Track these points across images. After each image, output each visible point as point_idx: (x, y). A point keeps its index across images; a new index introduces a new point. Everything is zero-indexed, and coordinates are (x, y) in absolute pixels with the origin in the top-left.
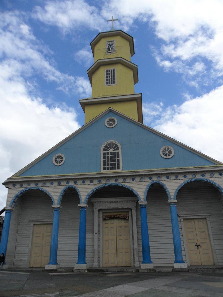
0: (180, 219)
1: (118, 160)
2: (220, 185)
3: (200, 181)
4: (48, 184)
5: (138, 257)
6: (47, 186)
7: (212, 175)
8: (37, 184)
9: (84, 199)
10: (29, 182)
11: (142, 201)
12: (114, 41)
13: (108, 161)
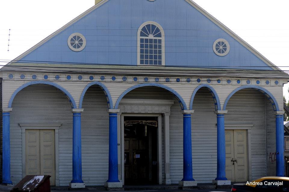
2: (274, 96)
6: (73, 79)
11: (188, 108)
13: (155, 52)
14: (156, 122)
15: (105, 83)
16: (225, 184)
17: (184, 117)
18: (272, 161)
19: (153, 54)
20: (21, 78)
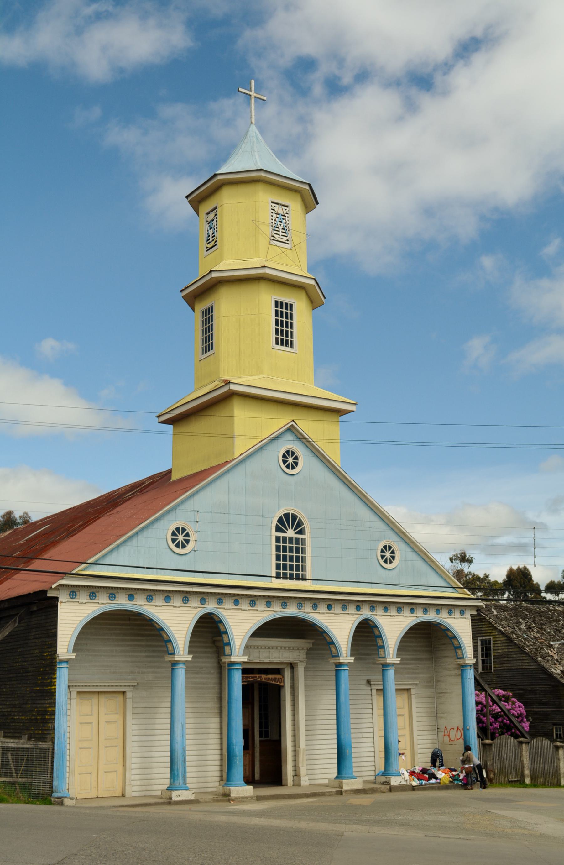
0: (371, 690)
2: (460, 634)
4: (323, 608)
9: (393, 646)
13: (285, 558)
14: (281, 677)
15: (224, 610)
16: (401, 784)
17: (336, 670)
18: (450, 740)
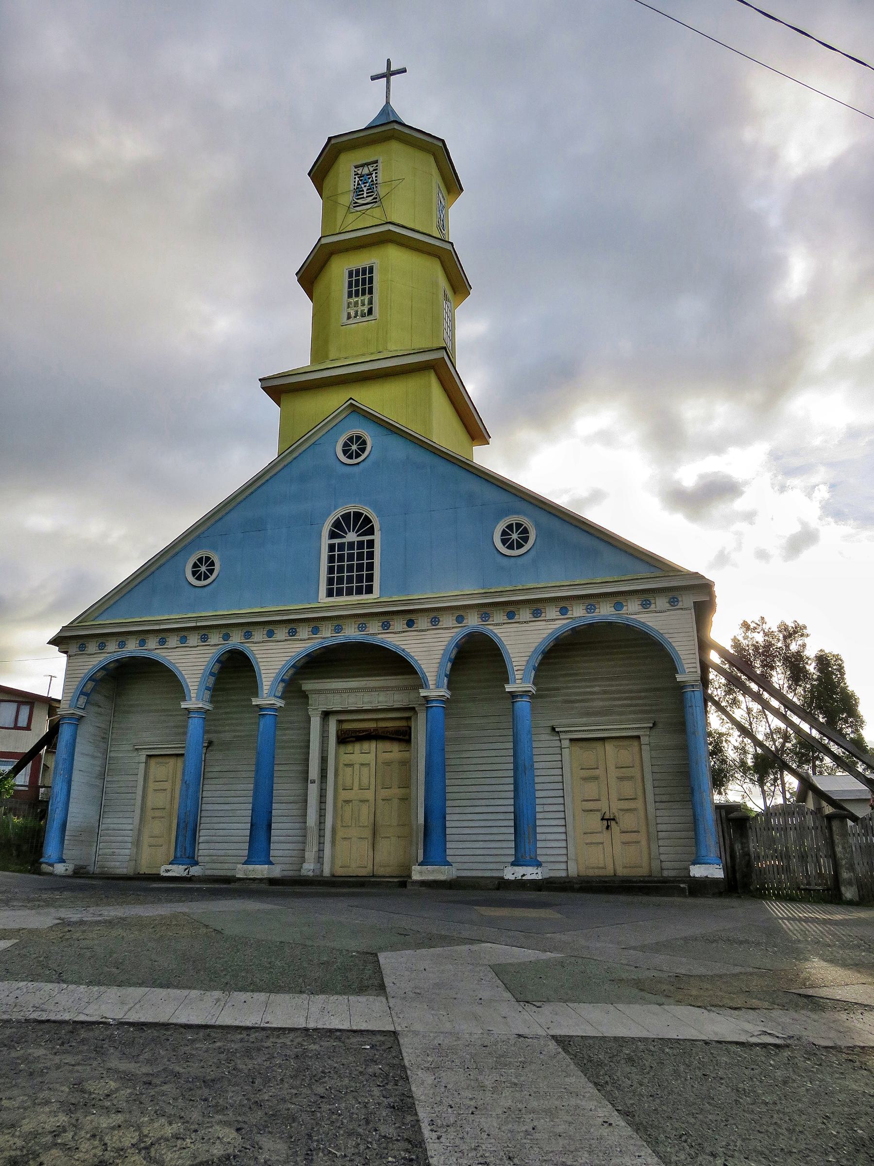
0: (560, 740)
1: (371, 567)
3: (610, 625)
4: (173, 641)
5: (167, 849)
7: (646, 604)
8: (142, 643)
10: (122, 637)
12: (376, 162)
15: (253, 645)
19: (355, 574)
20: (535, 617)
